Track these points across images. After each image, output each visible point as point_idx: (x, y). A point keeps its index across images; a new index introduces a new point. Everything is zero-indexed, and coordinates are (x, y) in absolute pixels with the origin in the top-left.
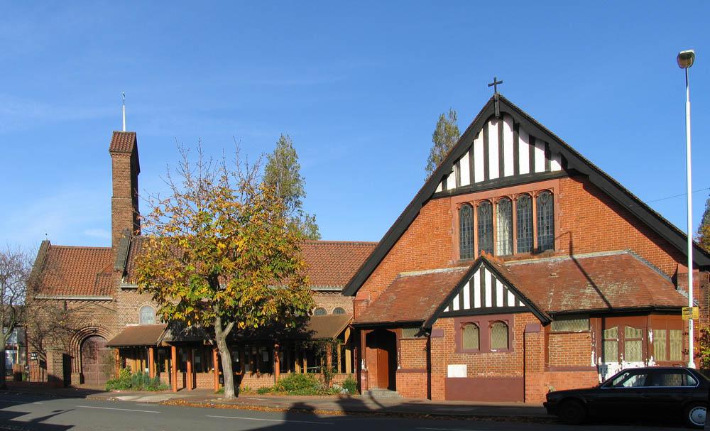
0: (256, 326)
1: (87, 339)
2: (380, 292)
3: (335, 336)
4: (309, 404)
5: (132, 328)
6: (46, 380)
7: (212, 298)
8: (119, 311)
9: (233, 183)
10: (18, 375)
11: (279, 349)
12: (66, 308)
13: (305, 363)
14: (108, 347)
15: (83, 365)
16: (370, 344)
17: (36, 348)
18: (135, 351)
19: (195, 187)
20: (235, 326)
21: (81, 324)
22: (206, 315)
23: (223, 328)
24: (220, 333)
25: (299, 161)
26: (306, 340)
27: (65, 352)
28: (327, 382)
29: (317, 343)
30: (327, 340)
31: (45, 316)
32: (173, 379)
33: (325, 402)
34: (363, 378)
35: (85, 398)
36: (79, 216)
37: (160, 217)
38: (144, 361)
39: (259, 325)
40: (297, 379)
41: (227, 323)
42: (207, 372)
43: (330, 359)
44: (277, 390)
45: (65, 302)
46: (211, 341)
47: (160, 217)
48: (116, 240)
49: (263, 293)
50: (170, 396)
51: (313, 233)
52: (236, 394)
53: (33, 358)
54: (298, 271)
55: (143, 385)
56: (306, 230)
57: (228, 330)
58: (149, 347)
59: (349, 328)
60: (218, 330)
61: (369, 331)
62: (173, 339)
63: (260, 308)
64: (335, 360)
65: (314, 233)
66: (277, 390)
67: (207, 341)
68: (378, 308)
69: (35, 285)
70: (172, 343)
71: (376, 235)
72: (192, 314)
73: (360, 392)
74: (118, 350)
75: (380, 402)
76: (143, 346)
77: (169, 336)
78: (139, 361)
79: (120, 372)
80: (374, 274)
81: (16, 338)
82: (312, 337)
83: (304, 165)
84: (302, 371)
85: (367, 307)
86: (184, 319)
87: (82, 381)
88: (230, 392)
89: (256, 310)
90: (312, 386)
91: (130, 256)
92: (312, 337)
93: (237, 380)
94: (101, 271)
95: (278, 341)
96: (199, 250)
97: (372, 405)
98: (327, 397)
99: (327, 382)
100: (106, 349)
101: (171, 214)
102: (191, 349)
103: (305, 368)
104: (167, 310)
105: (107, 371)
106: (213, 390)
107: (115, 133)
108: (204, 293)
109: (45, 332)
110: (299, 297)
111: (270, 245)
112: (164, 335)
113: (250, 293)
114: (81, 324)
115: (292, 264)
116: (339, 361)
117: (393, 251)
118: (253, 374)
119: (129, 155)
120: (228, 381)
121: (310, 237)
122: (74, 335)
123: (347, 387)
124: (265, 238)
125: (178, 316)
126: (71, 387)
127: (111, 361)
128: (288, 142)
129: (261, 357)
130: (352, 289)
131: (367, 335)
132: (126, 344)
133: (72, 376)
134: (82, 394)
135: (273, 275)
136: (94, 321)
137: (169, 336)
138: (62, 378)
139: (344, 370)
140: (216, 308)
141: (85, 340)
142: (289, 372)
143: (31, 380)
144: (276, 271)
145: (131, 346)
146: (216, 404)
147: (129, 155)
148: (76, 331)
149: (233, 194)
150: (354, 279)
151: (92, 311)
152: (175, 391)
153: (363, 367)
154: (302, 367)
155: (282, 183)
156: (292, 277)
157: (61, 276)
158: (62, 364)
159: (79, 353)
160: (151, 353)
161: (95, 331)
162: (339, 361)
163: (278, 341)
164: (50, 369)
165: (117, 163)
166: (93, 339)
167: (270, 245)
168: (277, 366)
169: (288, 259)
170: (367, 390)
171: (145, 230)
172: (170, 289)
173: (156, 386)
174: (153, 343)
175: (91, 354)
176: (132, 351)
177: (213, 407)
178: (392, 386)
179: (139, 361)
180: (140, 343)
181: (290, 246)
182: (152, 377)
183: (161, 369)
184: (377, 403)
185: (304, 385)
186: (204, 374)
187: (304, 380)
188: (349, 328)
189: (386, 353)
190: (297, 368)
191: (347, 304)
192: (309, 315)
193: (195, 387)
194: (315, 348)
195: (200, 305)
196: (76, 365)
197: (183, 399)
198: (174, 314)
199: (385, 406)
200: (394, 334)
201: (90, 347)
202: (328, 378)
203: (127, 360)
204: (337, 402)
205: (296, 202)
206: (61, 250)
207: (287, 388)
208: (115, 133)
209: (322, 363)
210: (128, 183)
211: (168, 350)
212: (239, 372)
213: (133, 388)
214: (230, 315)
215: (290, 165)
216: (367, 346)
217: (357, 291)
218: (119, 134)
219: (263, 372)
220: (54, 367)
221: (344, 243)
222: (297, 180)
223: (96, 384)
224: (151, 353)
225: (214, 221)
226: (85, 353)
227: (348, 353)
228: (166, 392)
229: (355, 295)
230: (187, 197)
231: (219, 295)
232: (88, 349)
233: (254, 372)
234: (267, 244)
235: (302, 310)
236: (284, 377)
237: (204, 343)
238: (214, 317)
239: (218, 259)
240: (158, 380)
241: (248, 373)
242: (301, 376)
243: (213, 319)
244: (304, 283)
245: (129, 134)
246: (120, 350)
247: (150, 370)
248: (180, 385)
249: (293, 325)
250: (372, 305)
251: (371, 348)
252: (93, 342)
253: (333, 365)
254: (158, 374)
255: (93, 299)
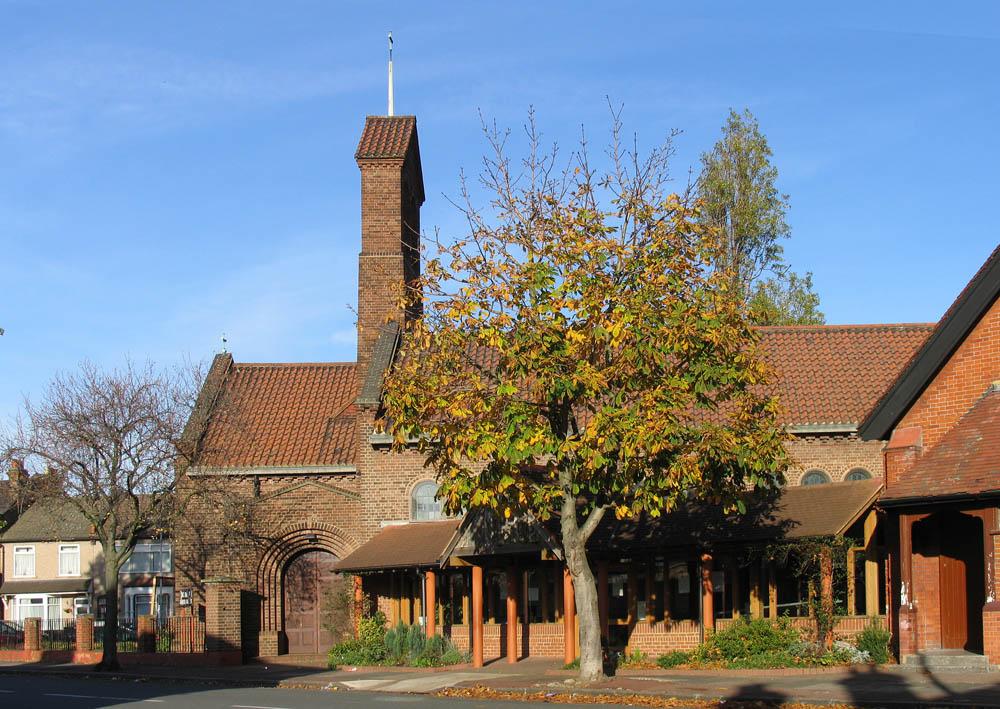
0: (655, 513)
1: (295, 556)
2: (946, 427)
3: (839, 530)
4: (774, 688)
5: (393, 529)
6: (199, 649)
7: (556, 454)
8: (365, 495)
9: (606, 202)
10: (149, 640)
11: (715, 566)
12: (258, 493)
13: (773, 594)
14: (337, 573)
15: (287, 613)
16: (922, 546)
17: (192, 579)
18: (397, 581)
19: (523, 214)
20: (610, 515)
21: (284, 527)
22: (541, 493)
23: (581, 521)
24: (573, 533)
25: (773, 161)
26: (773, 541)
27: (248, 588)
28: (821, 637)
29: (797, 546)
30: (821, 541)
31: (216, 518)
32: (479, 639)
33: (813, 682)
34: (904, 625)
35: (275, 684)
36: (300, 307)
37: (442, 282)
38: (417, 602)
39: (663, 511)
40: (751, 632)
41: (591, 510)
42: (552, 619)
43: (827, 583)
44: (705, 656)
45: (257, 480)
46: (557, 552)
47: (442, 282)
48: (367, 345)
49: (667, 437)
50: (465, 677)
51: (806, 312)
52: (609, 668)
53: (182, 602)
54: (755, 390)
55: (409, 655)
56: (792, 308)
57: (590, 526)
58: (425, 569)
59: (873, 513)
60: (568, 525)
61: (918, 517)
62: (477, 550)
63: (665, 471)
64: (840, 587)
65: (809, 311)
66: (705, 656)
67: (550, 553)
68: (939, 463)
69: (194, 448)
70: (474, 560)
71: (930, 307)
72: (512, 490)
73: (897, 657)
74: (359, 580)
75: (944, 680)
76: (412, 569)
77: (466, 543)
78: (407, 601)
79: (360, 625)
80: (932, 388)
81: (169, 561)
82: (788, 535)
83: (791, 169)
84: (767, 613)
85: (916, 462)
86: (495, 504)
87: (283, 646)
88: (592, 666)
89: (658, 476)
90: (786, 646)
91: (401, 381)
92: (788, 535)
93: (614, 641)
94: (336, 412)
95: (710, 548)
96: (523, 349)
97: (924, 690)
98: (820, 670)
99: (821, 637)
100: (333, 577)
101: (465, 274)
102: (511, 572)
103: (773, 607)
104: (459, 486)
105: (337, 624)
106: (564, 661)
107: (370, 121)
108: (537, 444)
109: (213, 546)
110: (752, 444)
111: (687, 330)
112: (455, 542)
113: (642, 435)
114: (284, 527)
115: (738, 369)
116: (851, 586)
117: (976, 333)
118: (653, 623)
119: (400, 165)
120: (589, 640)
121: (800, 321)
122: (269, 549)
123: (868, 648)
124: (675, 314)
125: (482, 497)
126: (262, 662)
127: (344, 603)
128: (747, 123)
129: (674, 583)
130: (880, 424)
131: (915, 527)
132: (376, 564)
133: (261, 638)
134: (271, 676)
135: (693, 396)
136: (313, 519)
137: (466, 543)
138: (238, 644)
139: (861, 608)
140: (565, 478)
141: (289, 563)
142: (736, 616)
143: (177, 649)
144: (700, 388)
145: (388, 570)
146: (558, 692)
147: (400, 165)
148: (273, 541)
149: (607, 223)
150: (885, 401)
151: (309, 497)
152: (478, 663)
153: (904, 599)
154: (766, 603)
155: (738, 208)
156: (737, 401)
157: (243, 426)
158: (239, 613)
159: (279, 587)
160: (430, 583)
161: (315, 540)
162: (851, 586)
163: (710, 548)
164: (213, 627)
165: (372, 181)
166: (311, 557)
167: (687, 330)
168: (707, 602)
169: (729, 359)
170: (916, 652)
171: (429, 322)
172: (460, 438)
173: (435, 655)
174: (433, 561)
175: (305, 590)
176: (390, 580)
177: (546, 701)
178: (975, 644)
179: (406, 602)
180: (407, 561)
181: (733, 332)
182: (430, 634)
183: (453, 618)
184: (937, 683)
185: (767, 643)
186: (548, 625)
187: (767, 633)
188: (873, 513)
189: (959, 567)
190: (755, 606)
191: (869, 457)
192: (777, 483)
193: (526, 653)
194: (794, 558)
195: (533, 474)
196: (270, 614)
197: (487, 683)
198: (473, 493)
199: (957, 690)
200: (979, 522)
201: (303, 575)
202: (824, 629)
203: (381, 600)
204: (843, 682)
205: (769, 250)
206: (252, 370)
207: (728, 651)
208: (370, 121)
209: (812, 592)
210: (395, 223)
211: (467, 573)
212: (624, 618)
213: (386, 662)
214: (599, 487)
215: (755, 171)
216: (914, 551)
217: (893, 426)
218: (379, 121)
219: (678, 617)
220: (222, 620)
221: (871, 329)
222: (770, 202)
223: (313, 655)
224: (430, 583)
225: (559, 284)
226: (291, 589)
227: (872, 568)
228: (458, 667)
229: (887, 436)
230: (506, 236)
231: (568, 447)
232: (299, 579)
233: (659, 618)
234: (679, 328)
235: (759, 474)
236: (723, 625)
237: (544, 558)
238: (560, 498)
239: (568, 367)
240: (442, 644)
241: (645, 620)
242: (760, 623)
243: (558, 503)
244: (768, 413)
245: (401, 121)
246: (365, 579)
247: (427, 618)
248: (492, 650)
249: (740, 507)
250: (929, 455)
251: (925, 555)
252: (309, 564)
253: (834, 596)
254: (447, 630)
255: (291, 472)
